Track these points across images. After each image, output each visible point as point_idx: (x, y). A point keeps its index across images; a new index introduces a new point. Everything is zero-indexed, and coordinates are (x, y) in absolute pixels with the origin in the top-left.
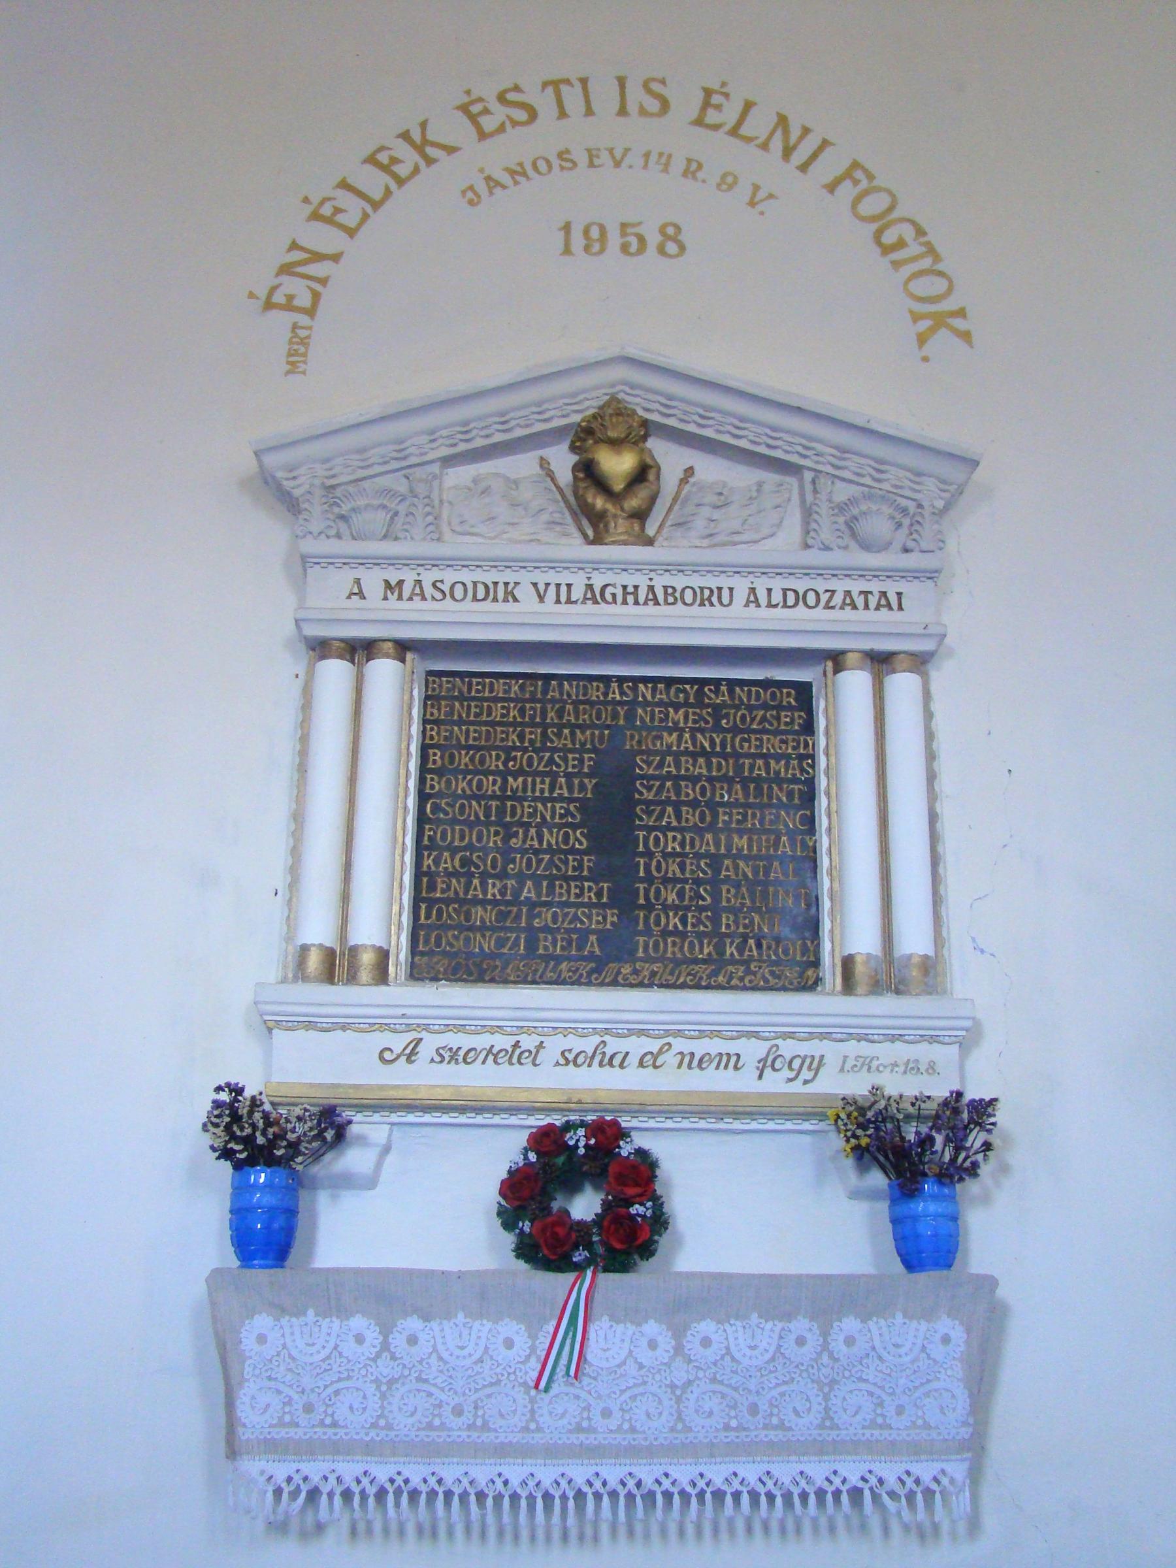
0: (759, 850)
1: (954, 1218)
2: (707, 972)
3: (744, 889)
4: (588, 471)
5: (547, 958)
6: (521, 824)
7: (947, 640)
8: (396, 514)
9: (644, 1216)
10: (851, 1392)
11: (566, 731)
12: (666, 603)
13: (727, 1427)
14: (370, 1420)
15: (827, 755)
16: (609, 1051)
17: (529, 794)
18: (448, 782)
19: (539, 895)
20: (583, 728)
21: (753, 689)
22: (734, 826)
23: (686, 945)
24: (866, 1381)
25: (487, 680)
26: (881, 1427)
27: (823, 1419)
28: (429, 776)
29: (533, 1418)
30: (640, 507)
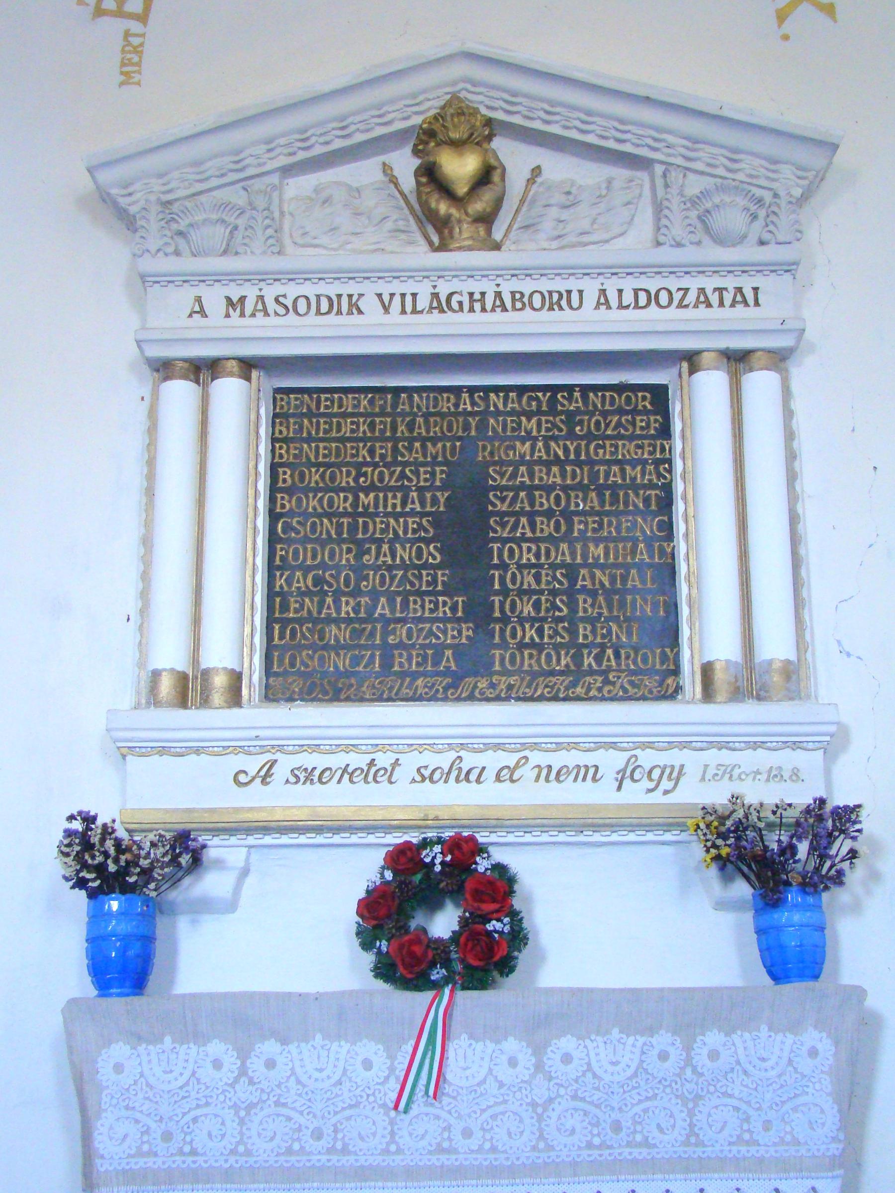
0: (616, 558)
1: (822, 929)
2: (565, 684)
3: (601, 598)
4: (430, 175)
5: (403, 675)
6: (373, 540)
7: (807, 334)
8: (236, 228)
9: (501, 933)
10: (716, 1107)
11: (417, 445)
12: (514, 308)
13: (590, 1145)
14: (230, 1147)
15: (684, 459)
16: (465, 767)
17: (381, 509)
18: (299, 500)
19: (393, 611)
20: (434, 440)
21: (607, 394)
22: (589, 534)
23: (543, 657)
24: (731, 1096)
25: (336, 396)
26: (747, 1143)
27: (688, 1136)
28: (279, 496)
29: (393, 1140)
30: (484, 210)
